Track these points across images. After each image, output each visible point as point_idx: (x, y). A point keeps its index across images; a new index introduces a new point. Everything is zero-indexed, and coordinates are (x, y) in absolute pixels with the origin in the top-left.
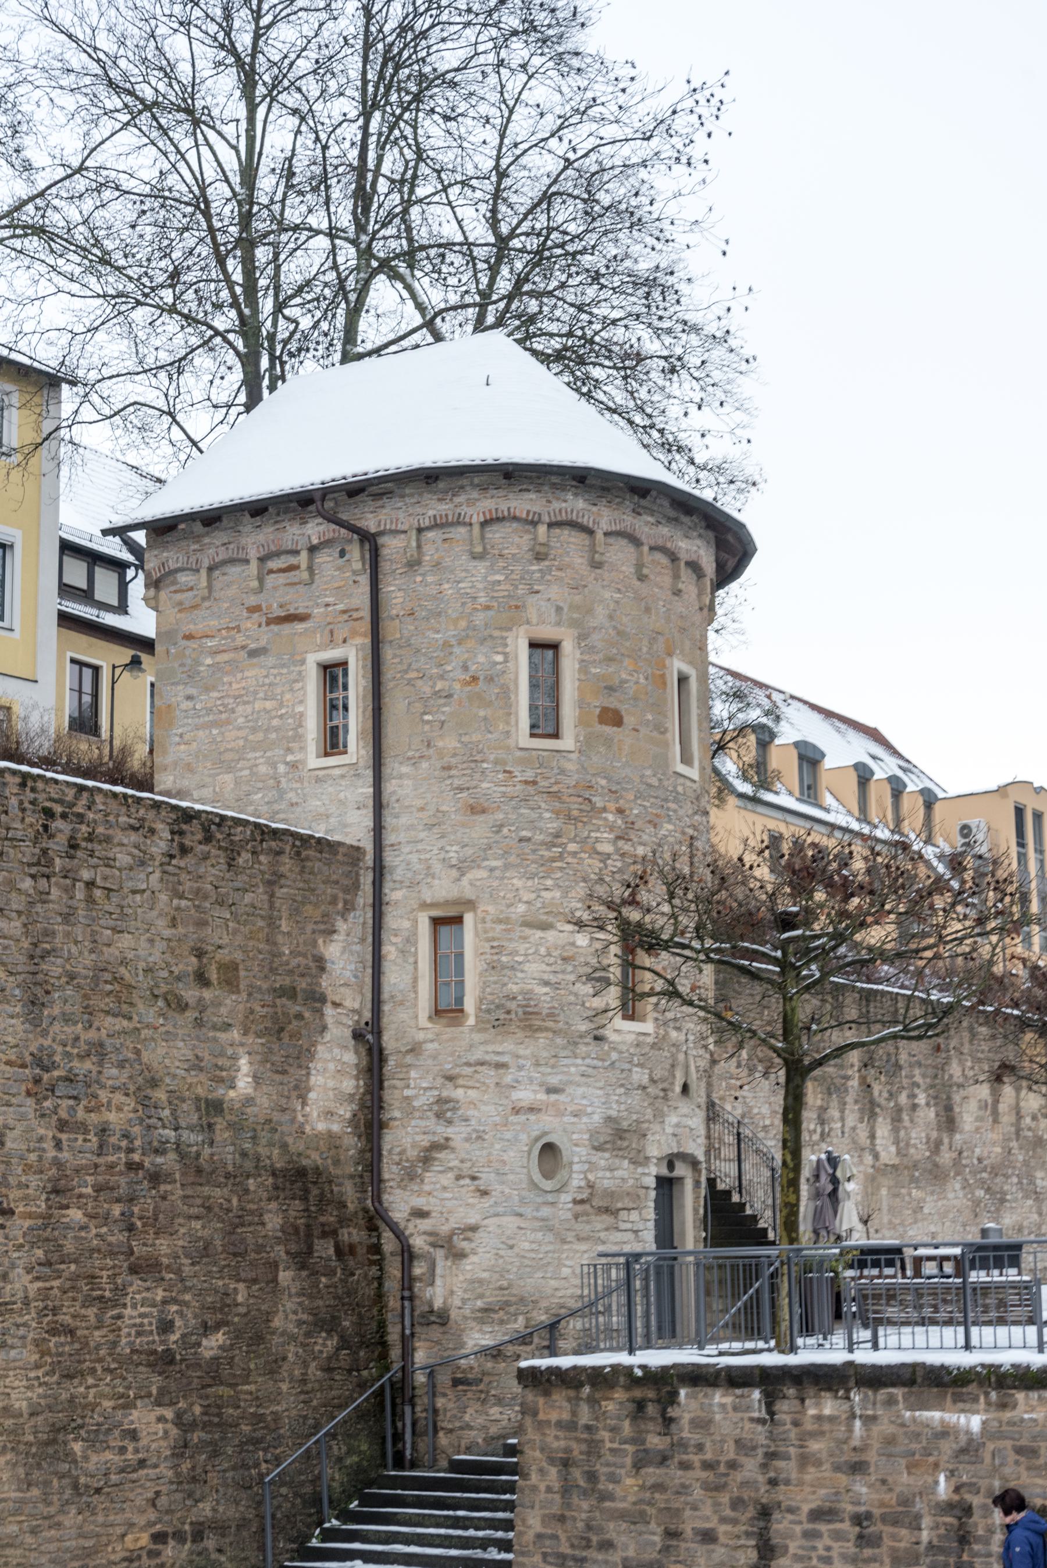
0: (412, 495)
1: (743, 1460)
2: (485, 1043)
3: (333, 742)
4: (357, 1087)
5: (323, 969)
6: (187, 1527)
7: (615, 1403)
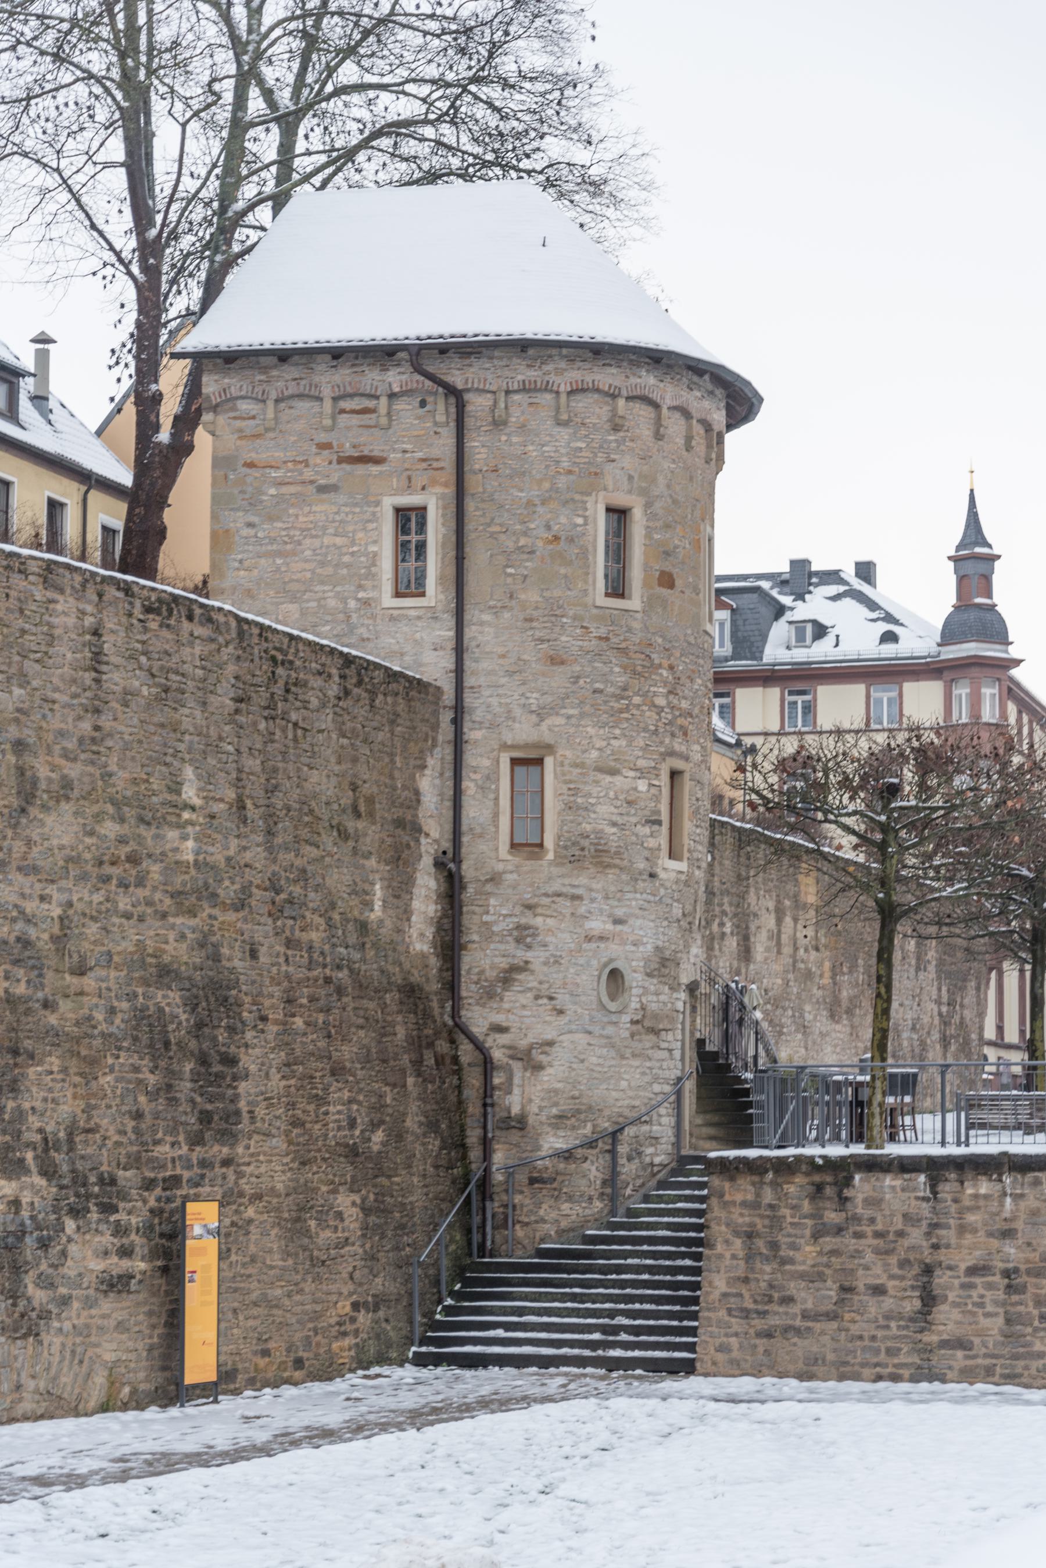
0: (501, 358)
1: (909, 1229)
2: (562, 876)
3: (409, 586)
4: (436, 911)
5: (418, 801)
6: (370, 1299)
7: (796, 1187)
